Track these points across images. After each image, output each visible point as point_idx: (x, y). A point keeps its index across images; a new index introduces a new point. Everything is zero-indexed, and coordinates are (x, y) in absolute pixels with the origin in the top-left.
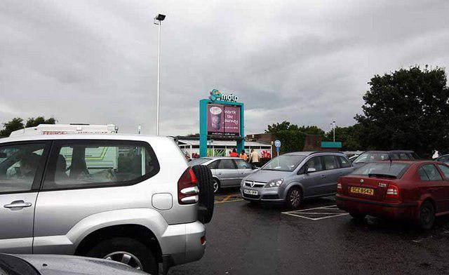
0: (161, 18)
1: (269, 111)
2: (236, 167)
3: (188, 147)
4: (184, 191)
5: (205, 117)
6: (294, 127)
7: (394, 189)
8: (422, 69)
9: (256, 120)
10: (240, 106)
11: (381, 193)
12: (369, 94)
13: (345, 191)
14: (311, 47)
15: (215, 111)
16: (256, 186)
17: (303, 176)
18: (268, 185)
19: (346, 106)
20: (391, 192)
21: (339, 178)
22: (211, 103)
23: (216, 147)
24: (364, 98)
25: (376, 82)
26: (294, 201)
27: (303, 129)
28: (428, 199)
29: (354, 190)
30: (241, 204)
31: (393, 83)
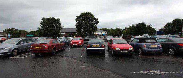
1: (5, 24)
8: (55, 18)
11: (43, 47)
13: (33, 48)
17: (19, 45)
19: (36, 25)
20: (46, 47)
27: (20, 31)
31: (48, 20)
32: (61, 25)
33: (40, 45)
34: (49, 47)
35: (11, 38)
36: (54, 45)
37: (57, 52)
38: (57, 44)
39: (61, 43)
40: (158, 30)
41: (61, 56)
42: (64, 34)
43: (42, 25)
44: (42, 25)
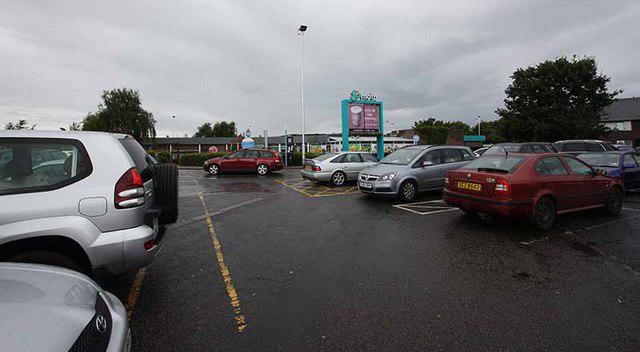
0: (303, 28)
1: (419, 110)
2: (362, 161)
3: (338, 143)
4: (121, 194)
5: (346, 116)
6: (439, 123)
7: (504, 184)
8: (570, 60)
9: (399, 118)
10: (378, 105)
11: (489, 189)
12: (512, 89)
13: (452, 186)
14: (454, 49)
15: (356, 110)
16: (370, 179)
17: (419, 170)
18: (381, 178)
19: (488, 103)
20: (500, 187)
21: (449, 173)
22: (352, 103)
23: (362, 142)
24: (506, 92)
25: (519, 75)
26: (408, 193)
27: (448, 125)
28: (548, 195)
29: (461, 185)
30: (358, 196)
31: (537, 76)
32: (603, 88)
33: (474, 179)
34: (516, 189)
35: (419, 144)
36: (543, 185)
37: (562, 221)
38: (563, 179)
39: (594, 173)
40: (160, 134)
41: (587, 249)
42: (626, 127)
43: (511, 99)
44: (511, 99)
